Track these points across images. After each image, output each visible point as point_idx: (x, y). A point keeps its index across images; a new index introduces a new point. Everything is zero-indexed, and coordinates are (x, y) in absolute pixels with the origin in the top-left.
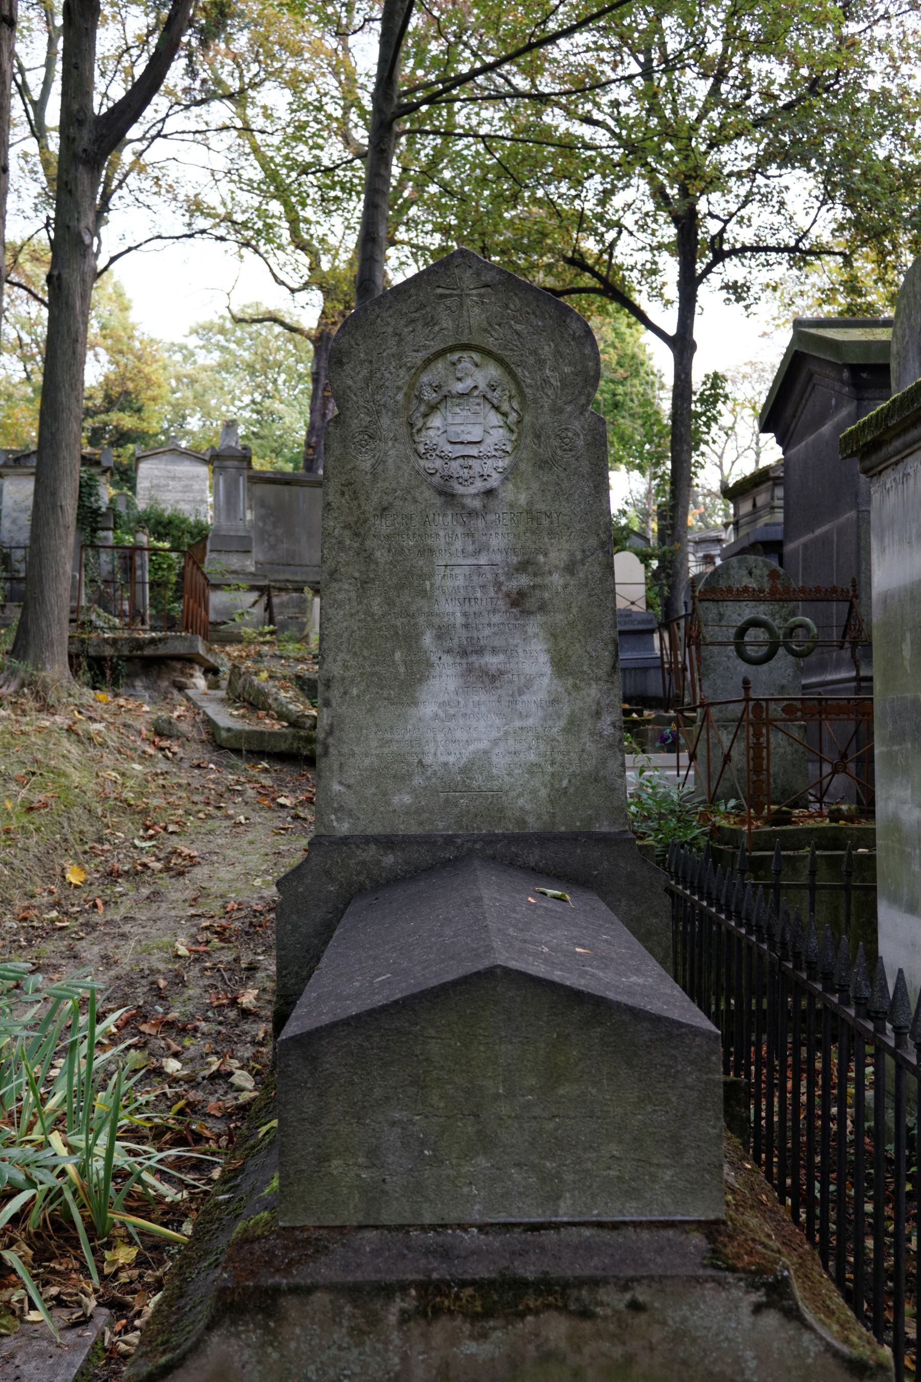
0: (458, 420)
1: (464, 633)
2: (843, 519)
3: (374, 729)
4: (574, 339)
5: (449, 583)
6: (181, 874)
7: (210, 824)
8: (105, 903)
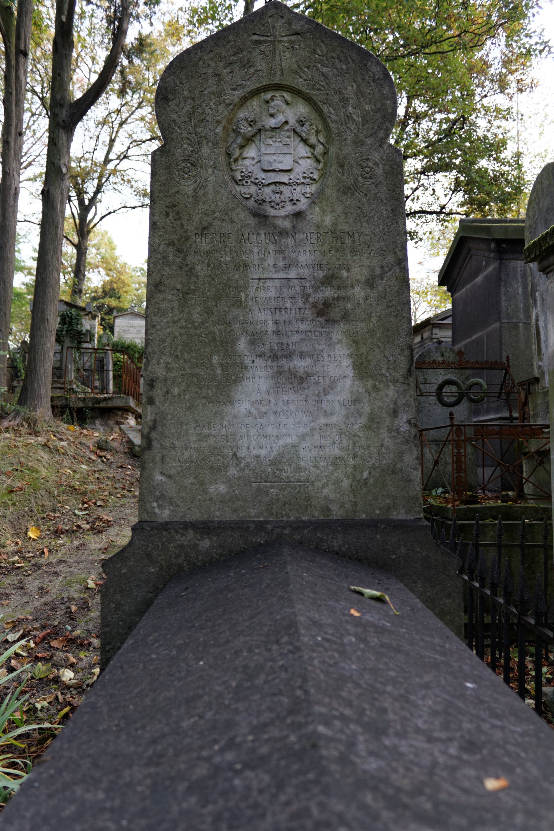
0: (271, 150)
1: (275, 339)
2: (490, 328)
3: (193, 425)
4: (374, 81)
5: (262, 294)
6: (100, 532)
7: (123, 501)
8: (50, 551)
